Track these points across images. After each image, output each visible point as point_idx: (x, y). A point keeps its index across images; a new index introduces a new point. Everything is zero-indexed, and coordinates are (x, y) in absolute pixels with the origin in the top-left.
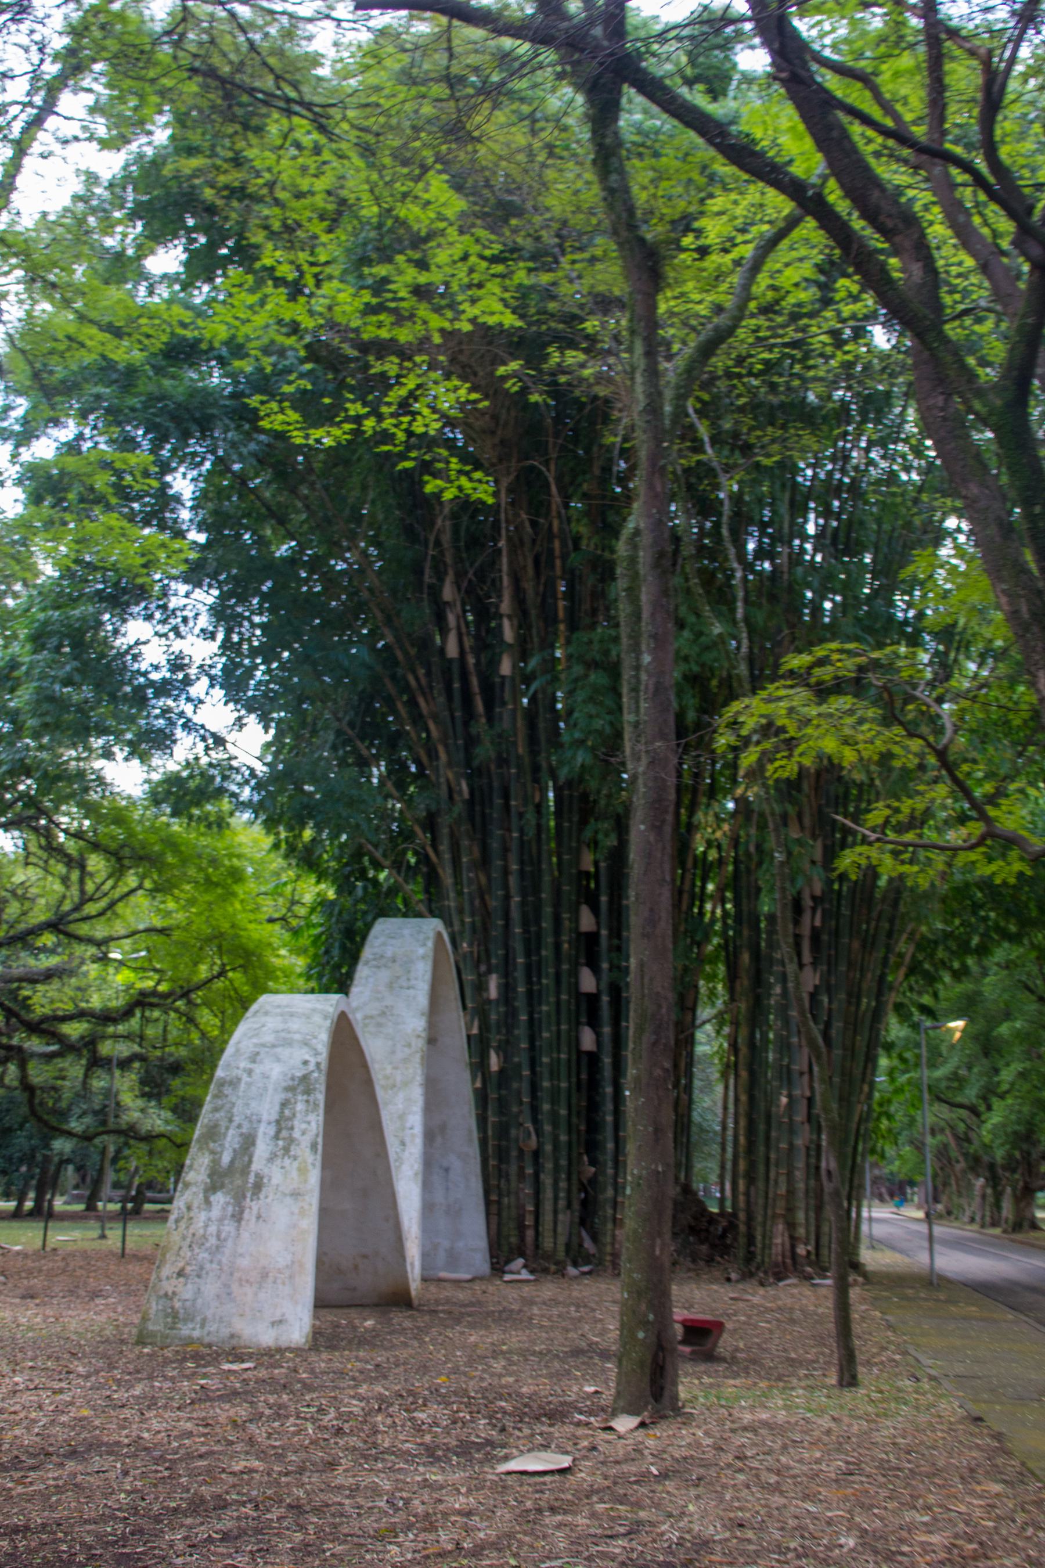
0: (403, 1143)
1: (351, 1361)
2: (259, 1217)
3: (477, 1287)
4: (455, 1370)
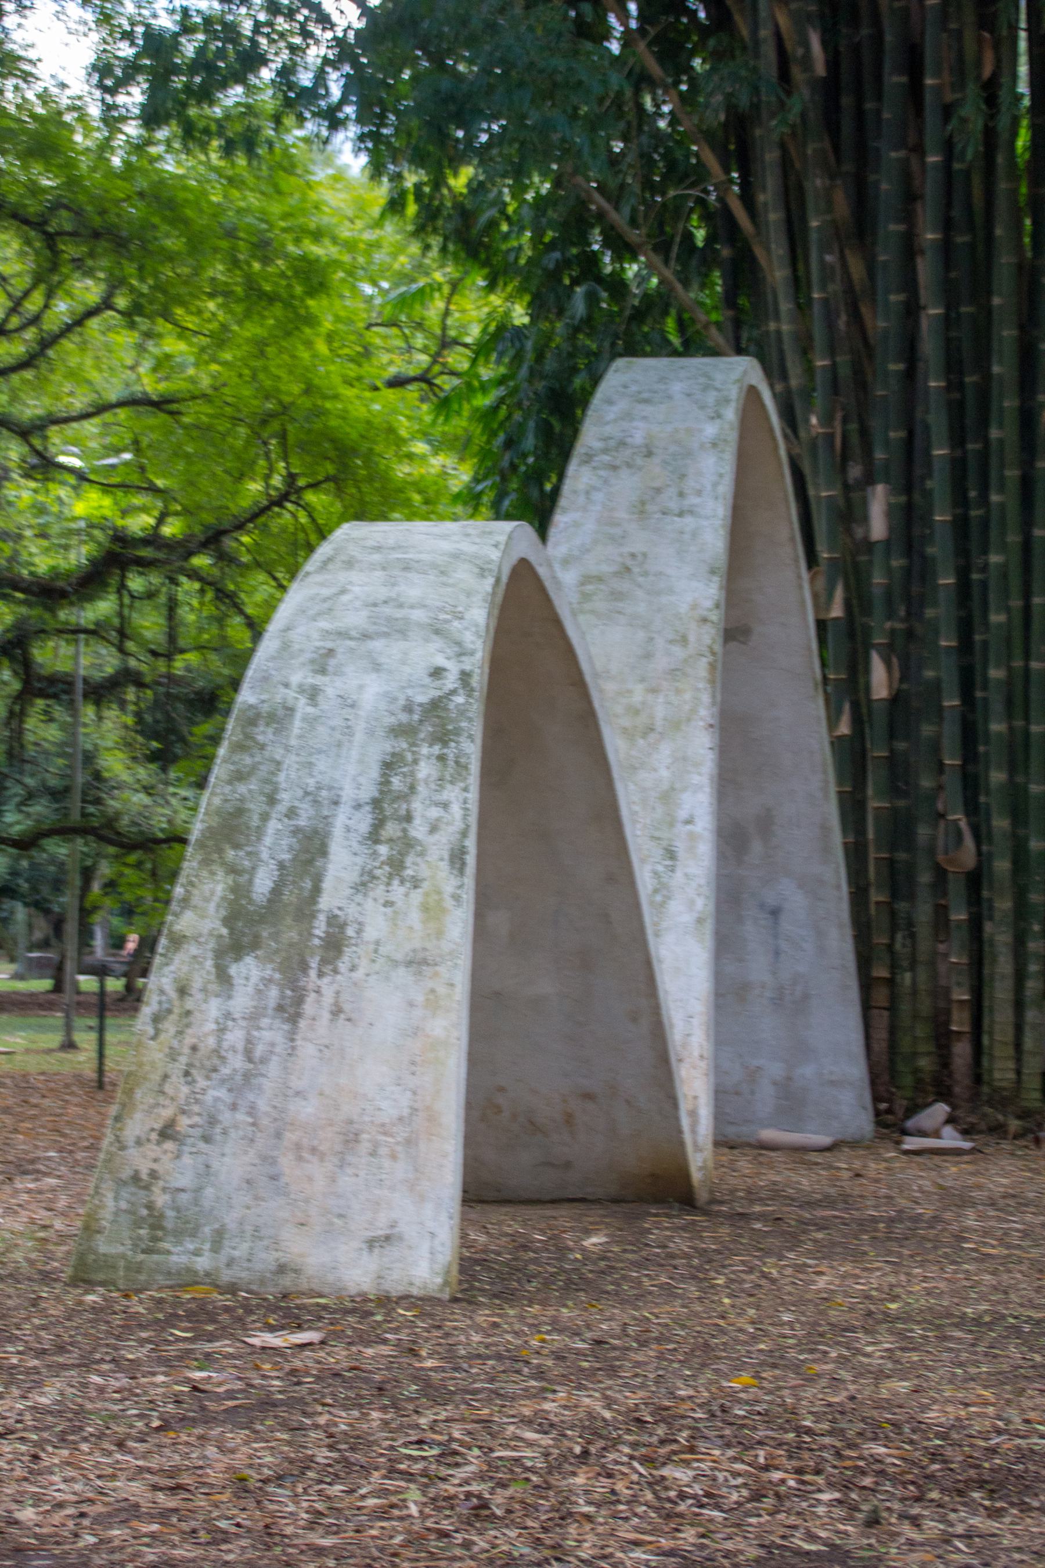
0: (671, 854)
1: (538, 1328)
2: (337, 1011)
3: (842, 1162)
4: (775, 1360)
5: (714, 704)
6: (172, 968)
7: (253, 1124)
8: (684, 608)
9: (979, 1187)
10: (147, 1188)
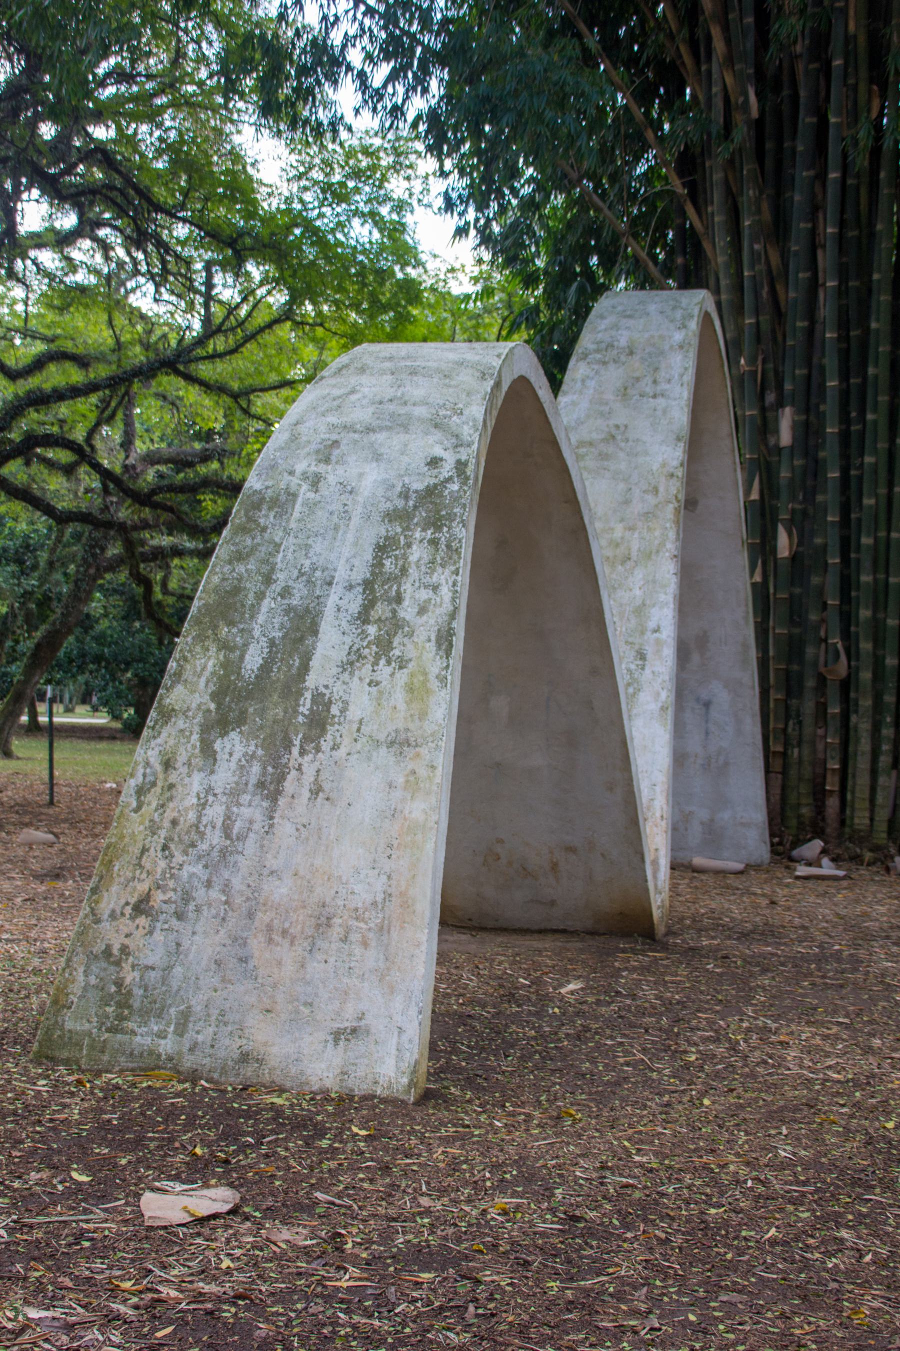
0: (642, 656)
2: (316, 790)
5: (677, 539)
6: (159, 741)
7: (226, 902)
8: (655, 467)
10: (118, 963)
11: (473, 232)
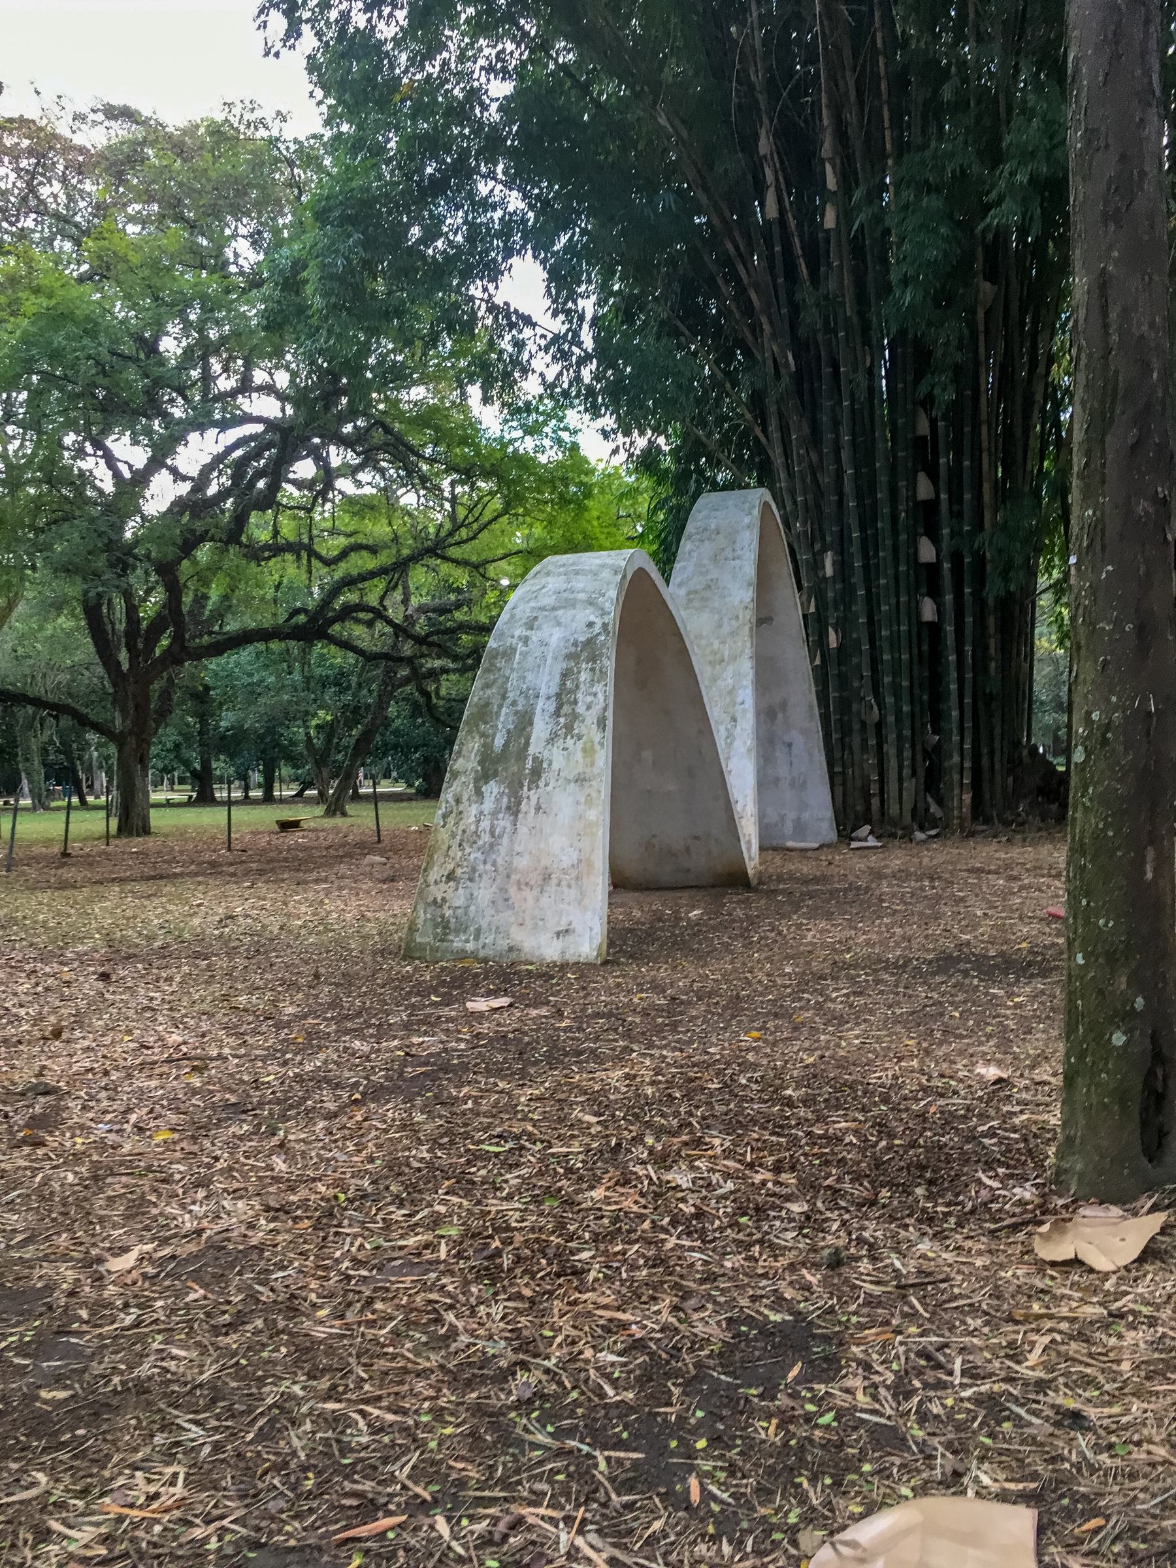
0: (734, 720)
2: (538, 808)
9: (886, 866)
11: (622, 450)
